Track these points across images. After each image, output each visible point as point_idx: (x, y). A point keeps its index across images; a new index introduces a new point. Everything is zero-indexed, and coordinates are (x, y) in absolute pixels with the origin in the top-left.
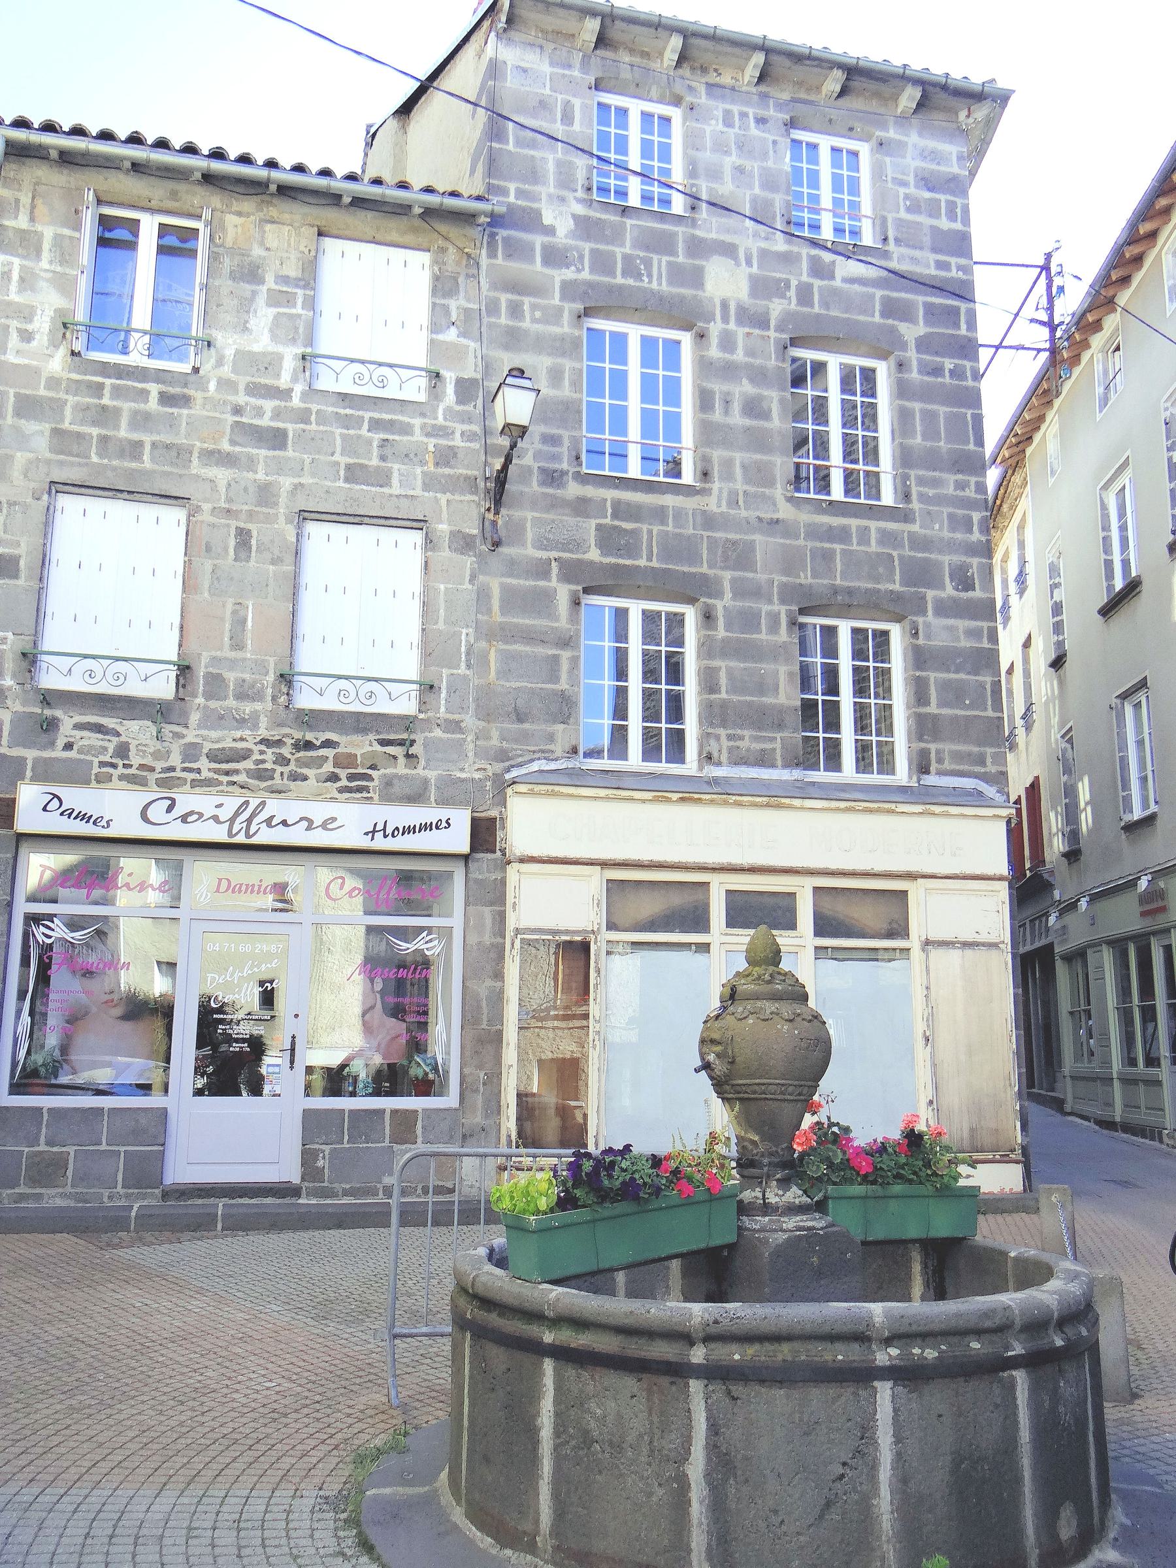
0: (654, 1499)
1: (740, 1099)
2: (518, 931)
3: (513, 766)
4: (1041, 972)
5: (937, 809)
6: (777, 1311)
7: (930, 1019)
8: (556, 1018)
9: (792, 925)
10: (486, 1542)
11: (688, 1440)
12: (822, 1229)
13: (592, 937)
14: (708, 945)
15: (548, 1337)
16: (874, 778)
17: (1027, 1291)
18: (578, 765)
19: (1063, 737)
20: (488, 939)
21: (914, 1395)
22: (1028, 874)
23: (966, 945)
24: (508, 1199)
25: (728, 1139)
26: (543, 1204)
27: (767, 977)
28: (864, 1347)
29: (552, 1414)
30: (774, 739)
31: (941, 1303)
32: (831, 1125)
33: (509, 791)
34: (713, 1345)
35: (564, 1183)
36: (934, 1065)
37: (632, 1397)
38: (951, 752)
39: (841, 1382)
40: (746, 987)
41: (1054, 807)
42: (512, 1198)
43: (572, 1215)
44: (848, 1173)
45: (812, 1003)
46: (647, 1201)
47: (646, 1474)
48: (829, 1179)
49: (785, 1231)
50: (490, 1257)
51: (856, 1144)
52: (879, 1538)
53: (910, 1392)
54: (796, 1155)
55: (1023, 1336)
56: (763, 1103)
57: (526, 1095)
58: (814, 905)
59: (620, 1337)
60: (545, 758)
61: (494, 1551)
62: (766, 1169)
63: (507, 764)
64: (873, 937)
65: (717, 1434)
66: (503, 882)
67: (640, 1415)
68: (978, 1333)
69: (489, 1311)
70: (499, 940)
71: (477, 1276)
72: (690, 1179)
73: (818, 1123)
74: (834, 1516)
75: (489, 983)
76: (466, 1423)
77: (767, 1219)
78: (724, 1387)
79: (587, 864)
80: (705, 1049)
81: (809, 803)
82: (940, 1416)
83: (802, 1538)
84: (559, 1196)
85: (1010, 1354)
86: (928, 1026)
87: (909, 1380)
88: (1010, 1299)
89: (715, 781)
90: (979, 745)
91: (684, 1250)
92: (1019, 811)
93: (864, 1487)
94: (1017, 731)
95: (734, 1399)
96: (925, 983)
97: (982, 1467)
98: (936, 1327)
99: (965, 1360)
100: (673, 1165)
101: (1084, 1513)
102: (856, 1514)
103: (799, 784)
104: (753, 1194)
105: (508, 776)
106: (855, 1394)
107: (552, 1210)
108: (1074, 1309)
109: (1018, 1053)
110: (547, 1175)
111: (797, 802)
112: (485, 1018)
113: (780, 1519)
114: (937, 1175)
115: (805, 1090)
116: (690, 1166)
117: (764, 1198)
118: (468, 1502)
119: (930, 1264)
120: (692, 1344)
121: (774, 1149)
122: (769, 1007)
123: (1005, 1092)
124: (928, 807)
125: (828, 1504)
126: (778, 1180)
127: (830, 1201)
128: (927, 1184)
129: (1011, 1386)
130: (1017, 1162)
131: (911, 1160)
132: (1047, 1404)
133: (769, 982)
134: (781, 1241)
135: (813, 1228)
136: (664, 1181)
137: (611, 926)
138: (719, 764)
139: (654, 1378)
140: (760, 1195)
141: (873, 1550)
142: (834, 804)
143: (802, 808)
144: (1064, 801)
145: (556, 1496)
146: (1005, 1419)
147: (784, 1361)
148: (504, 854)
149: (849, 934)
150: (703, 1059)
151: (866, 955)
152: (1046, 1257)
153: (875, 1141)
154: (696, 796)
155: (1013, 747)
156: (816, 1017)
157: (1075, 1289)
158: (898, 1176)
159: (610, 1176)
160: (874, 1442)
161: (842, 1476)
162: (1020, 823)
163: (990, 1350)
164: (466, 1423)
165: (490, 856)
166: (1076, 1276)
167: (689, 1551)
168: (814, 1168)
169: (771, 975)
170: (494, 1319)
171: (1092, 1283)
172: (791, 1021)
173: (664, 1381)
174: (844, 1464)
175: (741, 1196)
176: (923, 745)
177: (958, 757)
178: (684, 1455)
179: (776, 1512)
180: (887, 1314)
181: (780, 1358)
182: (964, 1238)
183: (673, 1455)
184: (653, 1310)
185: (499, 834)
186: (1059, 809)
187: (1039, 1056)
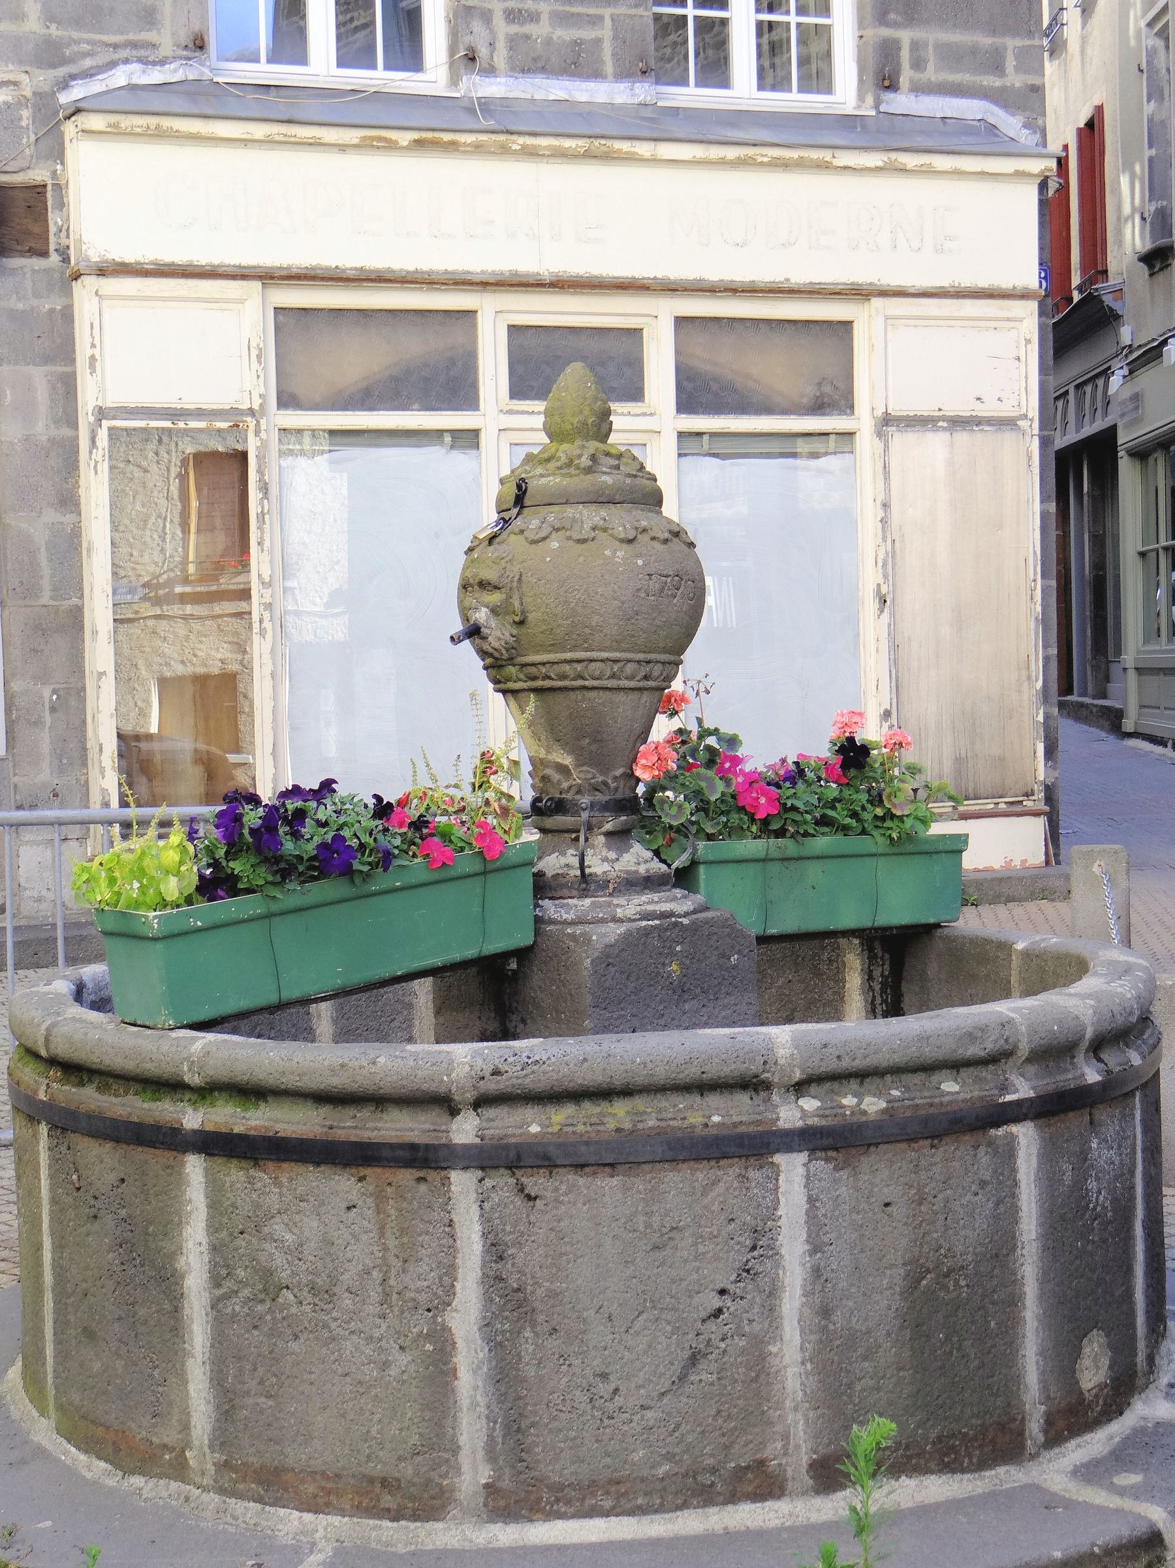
0: (393, 1372)
1: (536, 690)
2: (102, 413)
3: (73, 77)
4: (1092, 482)
5: (911, 161)
6: (605, 1047)
7: (890, 564)
8: (183, 599)
9: (635, 392)
10: (95, 1468)
11: (450, 1271)
12: (686, 915)
13: (251, 422)
14: (475, 433)
15: (192, 1119)
16: (793, 100)
17: (1043, 996)
18: (207, 74)
19: (1150, 25)
20: (42, 429)
21: (844, 1174)
22: (1076, 297)
23: (958, 423)
24: (103, 883)
25: (516, 763)
26: (172, 889)
27: (585, 461)
28: (758, 1100)
29: (204, 1248)
30: (596, 20)
31: (894, 1020)
32: (704, 733)
33: (69, 129)
34: (490, 1112)
35: (210, 851)
36: (895, 647)
37: (349, 1208)
38: (938, 46)
39: (718, 1159)
40: (542, 482)
41: (1128, 167)
42: (112, 881)
43: (228, 907)
44: (735, 818)
45: (669, 509)
46: (367, 876)
47: (377, 1333)
48: (700, 830)
49: (621, 921)
50: (79, 994)
51: (748, 767)
52: (779, 1405)
53: (837, 1169)
54: (641, 790)
55: (1032, 1069)
56: (579, 695)
57: (137, 738)
58: (678, 352)
59: (325, 1110)
60: (140, 60)
61: (111, 1482)
62: (585, 815)
63: (62, 71)
64: (785, 412)
65: (501, 1258)
66: (67, 315)
67: (364, 1237)
68: (956, 1066)
69: (81, 1084)
70: (66, 432)
71: (54, 1025)
72: (446, 836)
73: (680, 731)
74: (704, 1374)
75: (51, 516)
76: (48, 1278)
77: (587, 902)
78: (512, 1181)
79: (233, 277)
80: (470, 601)
81: (667, 150)
82: (887, 1205)
83: (649, 1414)
84: (201, 877)
85: (1009, 1098)
86: (885, 576)
87: (836, 1149)
88: (1013, 1010)
89: (487, 106)
90: (993, 32)
91: (437, 961)
92: (1062, 163)
93: (757, 1327)
94: (1066, 18)
95: (529, 1198)
96: (880, 498)
97: (957, 1282)
98: (883, 1059)
99: (932, 1110)
100: (413, 812)
101: (1122, 1346)
102: (742, 1370)
103: (647, 113)
104: (563, 861)
105: (64, 98)
106: (742, 1177)
107: (189, 901)
108: (1120, 1020)
109: (1045, 621)
110: (177, 836)
111: (644, 149)
112: (46, 584)
113: (613, 1386)
114: (893, 817)
115: (657, 670)
116: (445, 813)
117: (582, 867)
118: (60, 1408)
119: (877, 973)
120: (454, 1112)
121: (600, 779)
122: (591, 516)
123: (1020, 692)
124: (893, 156)
125: (694, 1359)
126: (608, 834)
127: (702, 869)
128: (876, 833)
129: (1008, 1154)
130: (1036, 814)
131: (847, 793)
132: (1068, 1178)
133: (589, 470)
134: (612, 939)
135: (671, 914)
136: (397, 841)
137: (286, 400)
138: (490, 71)
139: (387, 1174)
140: (575, 862)
141: (770, 1423)
142: (715, 152)
143: (654, 161)
144: (1148, 153)
145: (218, 1380)
146: (997, 1205)
147: (618, 1130)
148: (66, 260)
149: (743, 407)
150: (466, 619)
151: (775, 446)
152: (1076, 946)
153: (783, 761)
154: (447, 137)
155: (1057, 48)
156: (676, 534)
157: (1125, 990)
158: (824, 821)
159: (296, 835)
160: (773, 1253)
161: (719, 1311)
162: (1064, 189)
163: (976, 1094)
164: (48, 1278)
165: (36, 263)
166: (1127, 970)
167: (456, 1450)
168: (674, 811)
169: (593, 458)
170: (89, 1098)
171: (1152, 987)
172: (630, 541)
173: (406, 1177)
174: (722, 1292)
175: (540, 866)
176: (886, 32)
177: (952, 56)
178: (444, 1298)
179: (604, 1376)
180: (796, 1042)
181: (611, 1125)
182: (937, 926)
183: (423, 1298)
184: (382, 1060)
185: (54, 219)
186: (1138, 169)
187: (1083, 632)
